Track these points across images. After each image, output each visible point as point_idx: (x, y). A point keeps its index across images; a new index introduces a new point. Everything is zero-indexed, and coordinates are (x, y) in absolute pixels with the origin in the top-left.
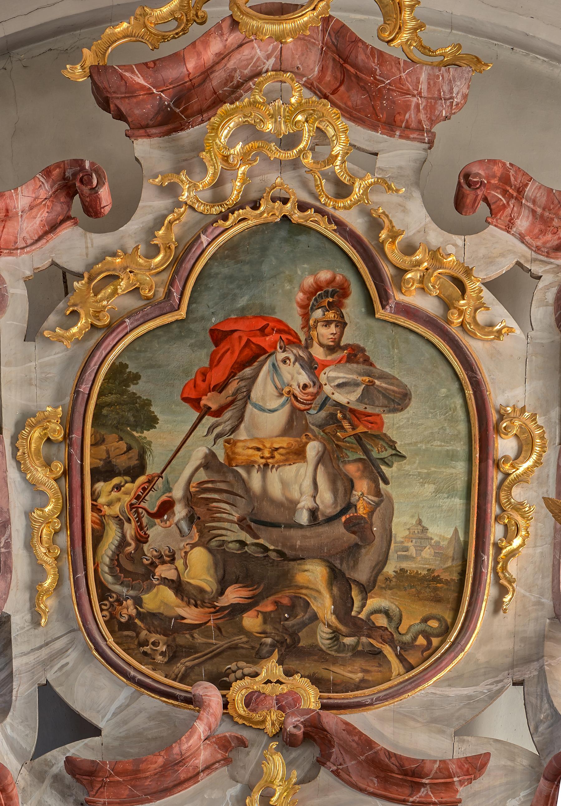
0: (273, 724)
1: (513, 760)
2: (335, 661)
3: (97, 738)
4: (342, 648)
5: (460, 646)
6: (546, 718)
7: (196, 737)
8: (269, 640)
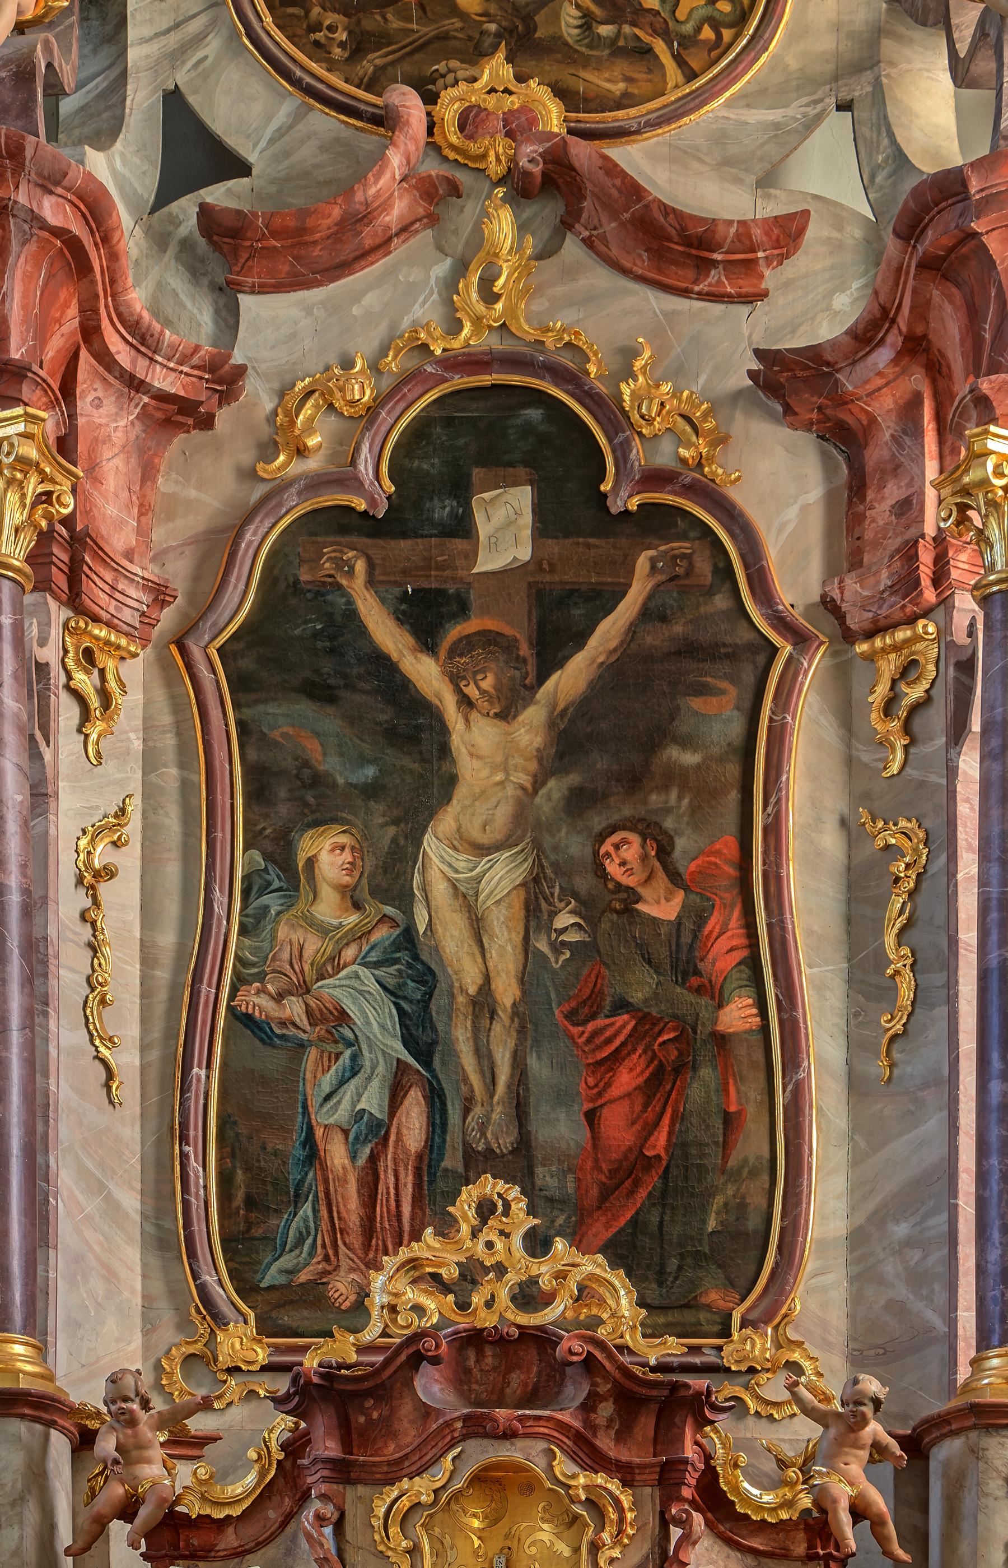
0: (498, 160)
1: (840, 229)
2: (585, 62)
3: (245, 180)
4: (598, 40)
5: (762, 42)
6: (886, 160)
7: (387, 175)
8: (493, 27)
